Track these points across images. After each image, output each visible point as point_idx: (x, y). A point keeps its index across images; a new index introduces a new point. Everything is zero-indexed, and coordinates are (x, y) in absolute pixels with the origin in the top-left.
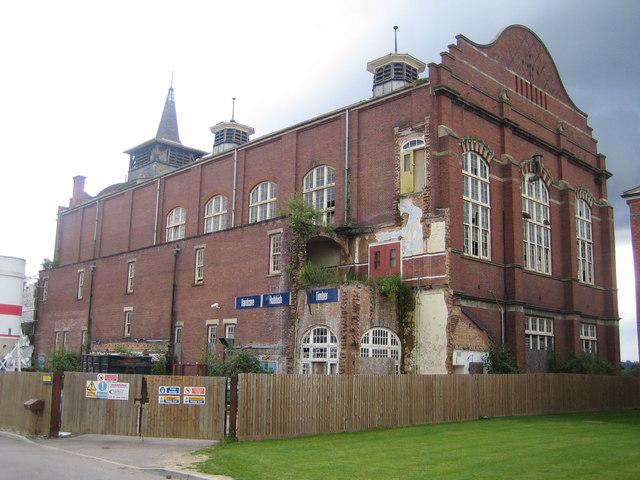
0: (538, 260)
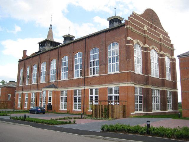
0: (155, 73)
